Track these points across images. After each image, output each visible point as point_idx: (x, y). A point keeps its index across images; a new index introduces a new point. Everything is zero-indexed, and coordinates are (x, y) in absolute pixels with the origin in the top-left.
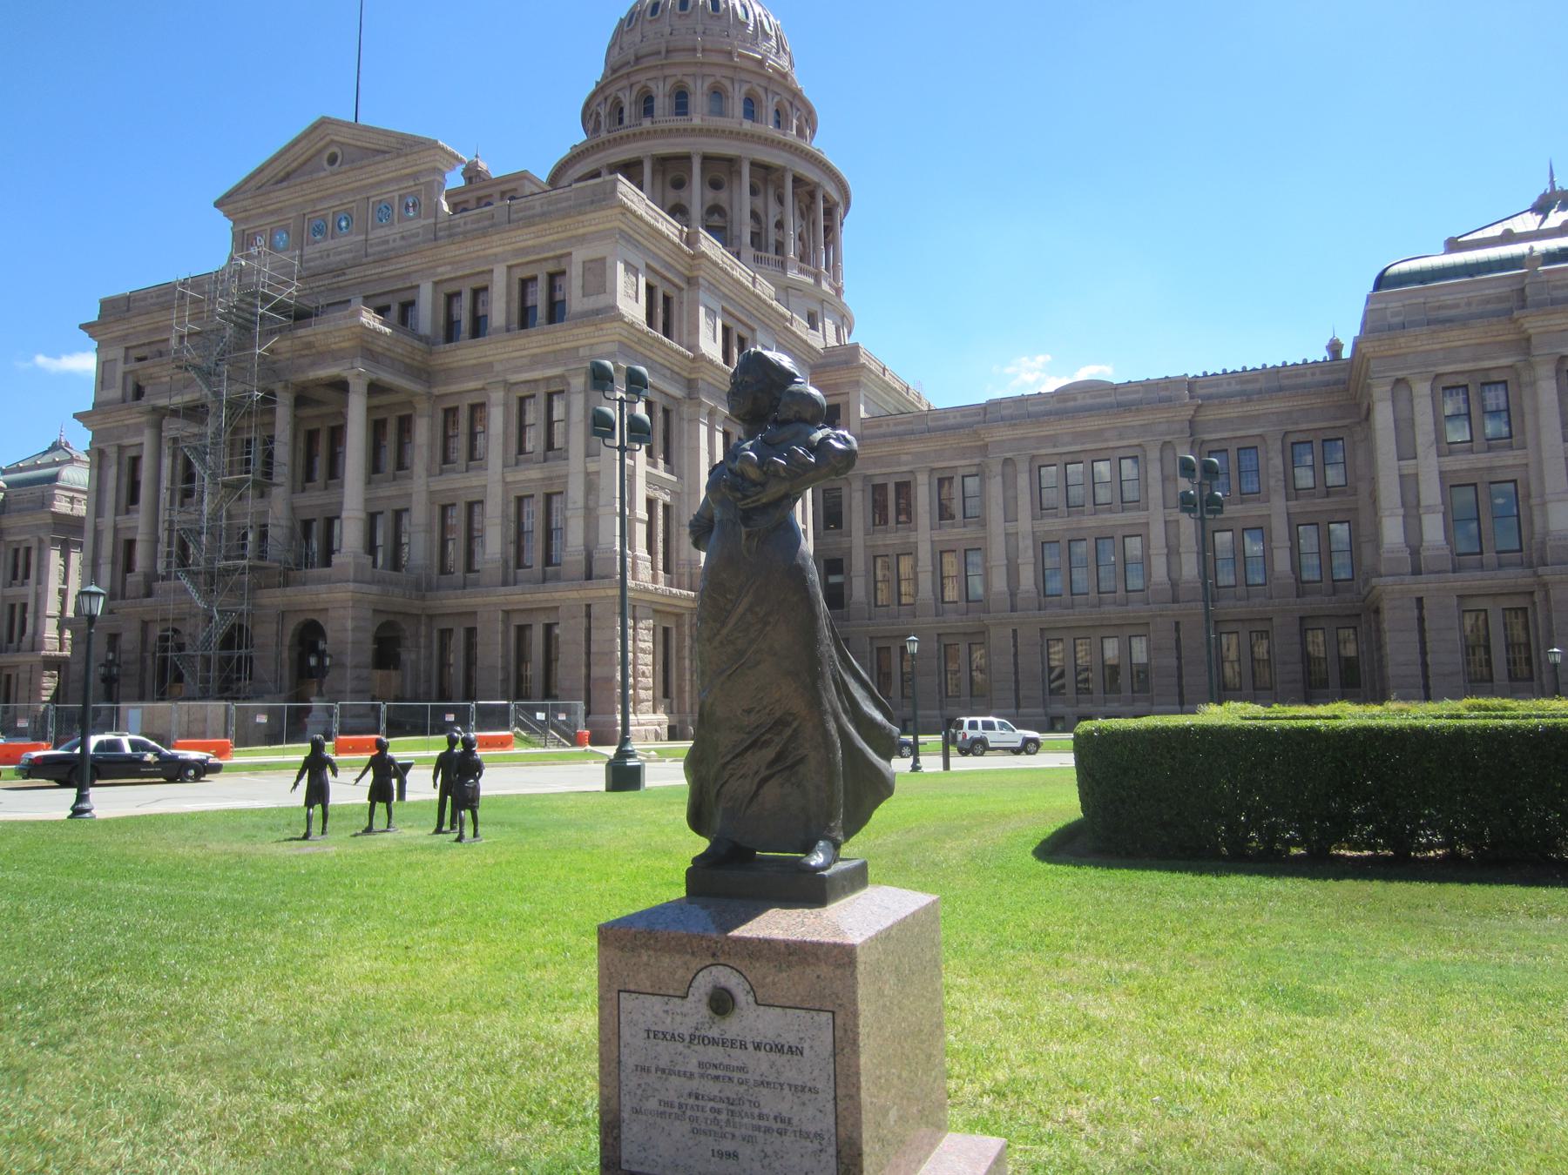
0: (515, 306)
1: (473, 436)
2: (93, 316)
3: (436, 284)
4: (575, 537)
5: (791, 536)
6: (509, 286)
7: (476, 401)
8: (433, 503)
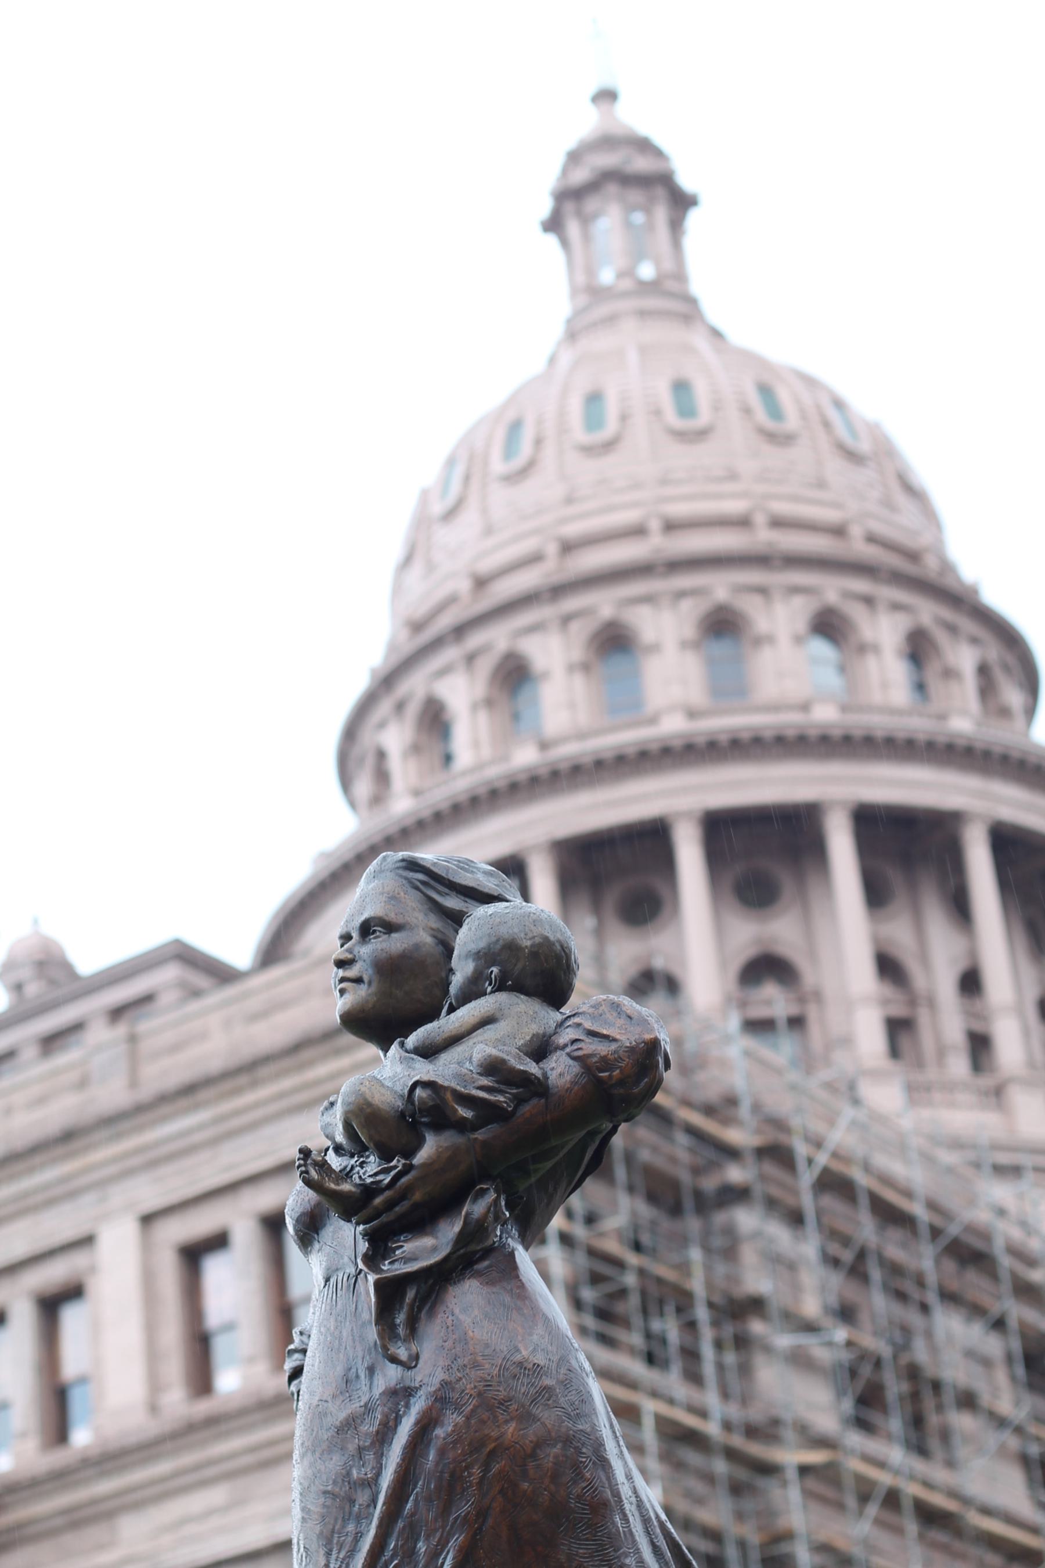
0: (172, 1333)
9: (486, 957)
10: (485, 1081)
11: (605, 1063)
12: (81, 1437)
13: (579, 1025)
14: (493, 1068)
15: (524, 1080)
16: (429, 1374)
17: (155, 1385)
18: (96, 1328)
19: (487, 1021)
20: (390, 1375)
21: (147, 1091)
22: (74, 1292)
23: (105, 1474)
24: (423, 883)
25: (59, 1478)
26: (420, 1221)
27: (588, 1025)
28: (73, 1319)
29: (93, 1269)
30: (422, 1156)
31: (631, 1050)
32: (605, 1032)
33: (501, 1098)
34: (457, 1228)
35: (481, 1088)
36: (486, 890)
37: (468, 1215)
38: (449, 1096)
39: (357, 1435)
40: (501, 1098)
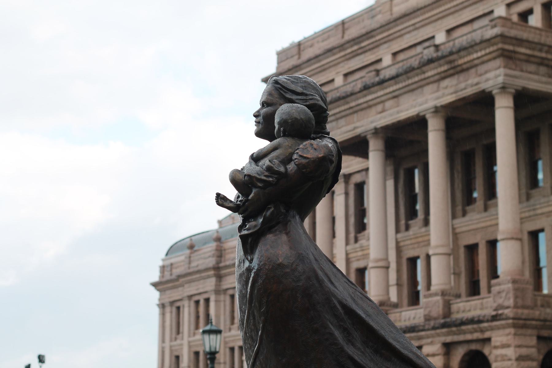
5: (272, 213)
9: (283, 123)
10: (267, 174)
13: (298, 153)
15: (278, 173)
16: (255, 264)
20: (247, 264)
21: (395, 15)
24: (280, 88)
27: (300, 153)
30: (250, 197)
32: (305, 156)
33: (271, 179)
35: (265, 176)
37: (265, 215)
38: (254, 179)
40: (271, 179)
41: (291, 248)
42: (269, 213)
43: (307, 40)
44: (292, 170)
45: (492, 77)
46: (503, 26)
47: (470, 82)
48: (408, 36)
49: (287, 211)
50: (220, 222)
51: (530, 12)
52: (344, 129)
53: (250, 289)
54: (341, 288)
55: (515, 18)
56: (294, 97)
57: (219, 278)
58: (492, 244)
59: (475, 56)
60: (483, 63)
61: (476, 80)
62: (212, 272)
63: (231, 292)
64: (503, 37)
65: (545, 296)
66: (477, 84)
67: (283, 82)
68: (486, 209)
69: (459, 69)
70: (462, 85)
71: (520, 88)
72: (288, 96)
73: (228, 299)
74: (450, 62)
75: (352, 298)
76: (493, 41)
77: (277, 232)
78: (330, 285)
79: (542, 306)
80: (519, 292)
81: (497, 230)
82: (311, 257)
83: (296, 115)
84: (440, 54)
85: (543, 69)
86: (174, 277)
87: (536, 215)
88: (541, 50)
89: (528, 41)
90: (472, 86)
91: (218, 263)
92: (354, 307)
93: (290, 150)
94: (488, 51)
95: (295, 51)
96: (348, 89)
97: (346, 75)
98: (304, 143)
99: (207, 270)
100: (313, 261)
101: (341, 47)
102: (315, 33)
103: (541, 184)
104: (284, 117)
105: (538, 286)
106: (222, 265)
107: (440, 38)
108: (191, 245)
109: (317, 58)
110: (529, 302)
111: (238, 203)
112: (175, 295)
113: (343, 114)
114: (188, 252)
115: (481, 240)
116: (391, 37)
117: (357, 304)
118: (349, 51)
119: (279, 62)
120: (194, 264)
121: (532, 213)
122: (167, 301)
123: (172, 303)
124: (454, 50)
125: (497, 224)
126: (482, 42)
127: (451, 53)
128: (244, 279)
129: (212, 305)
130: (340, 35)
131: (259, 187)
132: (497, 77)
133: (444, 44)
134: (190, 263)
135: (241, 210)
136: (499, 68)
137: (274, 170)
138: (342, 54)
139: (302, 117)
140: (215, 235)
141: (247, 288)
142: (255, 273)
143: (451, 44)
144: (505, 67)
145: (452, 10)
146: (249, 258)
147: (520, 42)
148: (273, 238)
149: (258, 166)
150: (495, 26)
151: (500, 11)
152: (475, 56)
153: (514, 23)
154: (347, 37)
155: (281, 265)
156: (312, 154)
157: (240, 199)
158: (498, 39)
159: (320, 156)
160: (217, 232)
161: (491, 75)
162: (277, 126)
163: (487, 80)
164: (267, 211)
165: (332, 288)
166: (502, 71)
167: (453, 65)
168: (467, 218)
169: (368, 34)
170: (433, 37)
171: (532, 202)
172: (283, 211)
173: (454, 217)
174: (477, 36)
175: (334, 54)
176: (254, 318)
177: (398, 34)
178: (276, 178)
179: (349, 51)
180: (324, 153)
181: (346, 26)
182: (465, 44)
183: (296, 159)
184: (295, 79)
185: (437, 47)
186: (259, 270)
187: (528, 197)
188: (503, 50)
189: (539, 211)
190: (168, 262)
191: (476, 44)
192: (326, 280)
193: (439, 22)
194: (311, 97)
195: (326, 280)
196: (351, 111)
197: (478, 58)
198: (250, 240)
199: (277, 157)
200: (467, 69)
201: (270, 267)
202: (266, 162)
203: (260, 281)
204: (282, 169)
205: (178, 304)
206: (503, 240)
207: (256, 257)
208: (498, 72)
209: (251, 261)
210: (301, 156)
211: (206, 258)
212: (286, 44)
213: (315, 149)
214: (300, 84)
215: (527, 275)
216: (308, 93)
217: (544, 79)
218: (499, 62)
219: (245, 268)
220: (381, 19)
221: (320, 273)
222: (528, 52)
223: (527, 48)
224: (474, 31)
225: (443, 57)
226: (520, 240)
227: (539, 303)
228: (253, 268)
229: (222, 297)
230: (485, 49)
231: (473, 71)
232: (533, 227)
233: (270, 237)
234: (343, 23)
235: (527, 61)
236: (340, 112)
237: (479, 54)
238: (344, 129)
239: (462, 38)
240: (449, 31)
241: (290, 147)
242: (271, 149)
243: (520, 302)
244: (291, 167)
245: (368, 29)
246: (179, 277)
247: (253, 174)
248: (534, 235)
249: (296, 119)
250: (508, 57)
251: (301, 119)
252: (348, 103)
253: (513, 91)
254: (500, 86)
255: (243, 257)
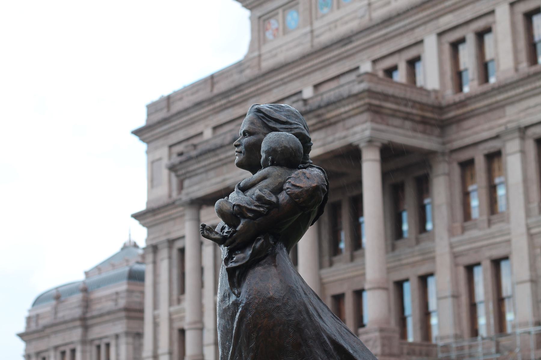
0: (522, 44)
1: (492, 189)
2: (141, 120)
3: (440, 35)
4: (164, 266)
5: (262, 245)
6: (513, 24)
7: (493, 150)
8: (456, 265)
9: (272, 152)
10: (257, 203)
11: (297, 196)
12: (492, 80)
13: (290, 182)
14: (260, 199)
15: (269, 203)
16: (243, 298)
17: (517, 62)
18: (496, 42)
19: (264, 178)
20: (233, 298)
22: (488, 30)
23: (500, 93)
24: (263, 117)
25: (484, 95)
26: (242, 248)
27: (293, 182)
28: (488, 39)
29: (494, 22)
30: (238, 229)
31: (307, 191)
32: (298, 185)
33: (262, 209)
34: (250, 252)
35: (255, 206)
36: (282, 120)
37: (254, 247)
38: (244, 210)
39: (228, 313)
40: (262, 209)
41: (281, 281)
42: (258, 245)
43: (176, 93)
44: (283, 200)
45: (360, 130)
46: (370, 81)
47: (338, 135)
48: (275, 91)
49: (275, 243)
50: (87, 273)
51: (395, 68)
52: (214, 181)
53: (237, 325)
54: (329, 323)
55: (381, 74)
56: (278, 126)
57: (86, 328)
58: (359, 294)
59: (342, 110)
60: (350, 117)
61: (344, 133)
62: (78, 323)
63: (97, 342)
64: (370, 92)
65: (411, 344)
66: (345, 137)
67: (266, 110)
68: (352, 258)
69: (327, 123)
70: (330, 139)
71: (386, 142)
72: (272, 124)
73: (94, 350)
74: (318, 116)
75: (339, 333)
76: (360, 96)
77: (266, 265)
78: (319, 320)
79: (408, 354)
80: (386, 340)
81: (364, 279)
82: (301, 290)
83: (285, 144)
84: (308, 108)
85: (408, 124)
86: (40, 327)
87: (402, 265)
88: (406, 105)
89: (393, 96)
90: (340, 139)
91: (85, 313)
92: (342, 342)
93: (280, 180)
94: (355, 105)
95: (164, 104)
96: (218, 141)
97: (215, 128)
98: (296, 172)
99: (73, 320)
100: (303, 295)
101: (210, 101)
102: (185, 87)
103: (406, 235)
104: (273, 145)
105: (404, 335)
106: (89, 315)
107: (308, 93)
108: (58, 296)
109: (186, 111)
110: (395, 350)
111: (225, 234)
112: (41, 345)
113: (212, 166)
114: (53, 302)
115: (347, 290)
116: (259, 92)
117: (344, 340)
118: (218, 104)
119: (149, 114)
120: (60, 315)
121: (397, 263)
122: (32, 351)
123: (38, 354)
124: (322, 104)
125: (364, 275)
126: (350, 96)
127: (319, 107)
128: (229, 313)
129: (113, 350)
130: (209, 89)
131: (249, 218)
132: (363, 131)
133: (311, 98)
134: (56, 313)
135: (227, 241)
136: (365, 122)
137: (265, 200)
138: (211, 107)
139: (291, 145)
140: (82, 286)
141: (233, 323)
142: (243, 307)
143: (319, 98)
144: (372, 121)
145: (320, 66)
146: (236, 292)
147: (386, 97)
148: (262, 270)
149: (246, 196)
150: (361, 82)
151: (366, 67)
152: (342, 110)
153: (380, 79)
154: (216, 91)
155: (271, 299)
156: (304, 184)
157: (226, 230)
158: (366, 94)
159: (313, 185)
160: (84, 282)
161: (358, 129)
162: (263, 155)
163: (355, 133)
164: (256, 243)
165: (321, 323)
166: (368, 125)
167: (320, 119)
168: (334, 268)
169: (237, 89)
170: (300, 92)
171: (397, 252)
172: (272, 242)
173: (321, 266)
174: (345, 91)
175: (203, 107)
176: (241, 355)
177: (267, 88)
178: (267, 208)
179: (218, 104)
180: (318, 183)
181: (215, 80)
182: (333, 98)
183: (288, 188)
184: (277, 107)
185: (305, 101)
186: (247, 305)
187: (393, 248)
188: (370, 105)
189: (405, 262)
190: (34, 313)
191: (344, 99)
192: (315, 314)
193: (306, 77)
194: (295, 126)
195: (315, 314)
196: (220, 163)
197: (346, 112)
198: (237, 273)
199: (267, 187)
200: (335, 123)
201: (261, 301)
202: (256, 191)
203: (249, 316)
204: (274, 199)
205: (43, 355)
206: (370, 289)
207: (244, 289)
208: (364, 126)
209: (238, 295)
210: (293, 185)
211: (72, 308)
212: (155, 97)
213: (308, 178)
214: (283, 113)
215: (393, 324)
216: (293, 122)
217: (410, 133)
218: (366, 116)
219: (231, 302)
220: (249, 73)
221: (310, 308)
222: (394, 106)
223: (392, 102)
224: (342, 86)
225: (311, 111)
226: (386, 289)
227: (405, 351)
228: (241, 303)
229: (88, 348)
230: (352, 103)
231: (340, 125)
232: (398, 276)
233: (259, 270)
234: (212, 77)
235: (393, 116)
236: (210, 164)
237: (347, 108)
238: (214, 181)
239: (330, 92)
240: (316, 87)
241: (280, 177)
242: (259, 178)
243: (387, 351)
244: (283, 197)
245: (237, 83)
246: (45, 327)
247: (243, 204)
248: (399, 285)
249: (285, 147)
250: (375, 111)
251: (291, 147)
252: (217, 155)
253: (379, 144)
254: (368, 139)
255: (229, 291)
